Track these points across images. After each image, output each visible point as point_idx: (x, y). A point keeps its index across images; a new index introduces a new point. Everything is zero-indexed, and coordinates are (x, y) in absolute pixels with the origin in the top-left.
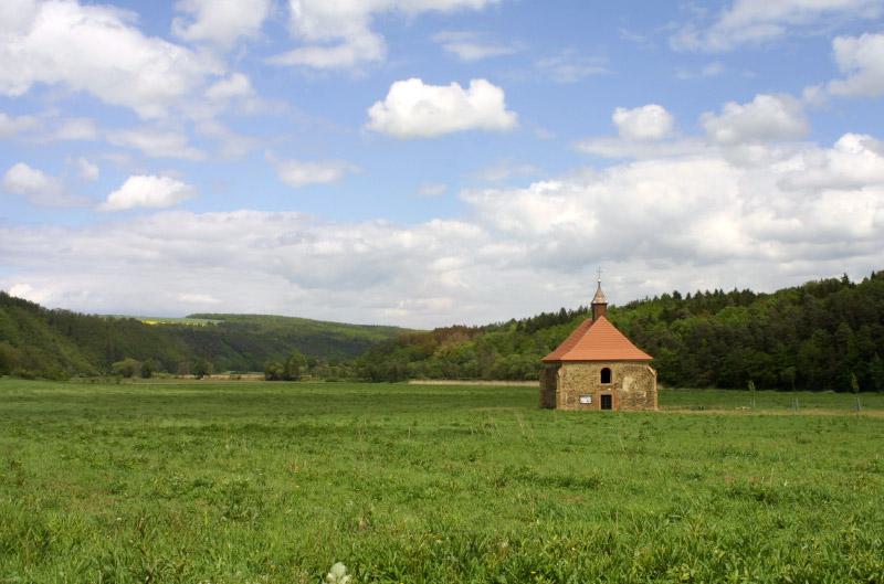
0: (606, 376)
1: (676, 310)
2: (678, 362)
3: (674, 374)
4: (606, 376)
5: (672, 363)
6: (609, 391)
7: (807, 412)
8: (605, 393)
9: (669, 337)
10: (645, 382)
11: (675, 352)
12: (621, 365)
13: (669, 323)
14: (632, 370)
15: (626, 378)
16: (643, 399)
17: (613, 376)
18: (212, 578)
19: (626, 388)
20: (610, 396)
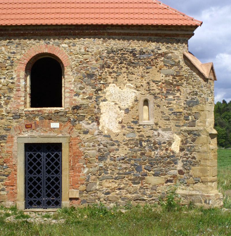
0: (46, 81)
1: (224, 107)
2: (226, 134)
3: (224, 140)
4: (46, 81)
5: (222, 135)
6: (52, 131)
7: (10, 187)
8: (37, 136)
9: (221, 121)
10: (178, 101)
11: (224, 129)
12: (97, 45)
13: (221, 114)
14: (134, 60)
15: (112, 89)
16: (172, 159)
17: (69, 82)
18: (110, 219)
19: (110, 120)
20: (58, 147)
